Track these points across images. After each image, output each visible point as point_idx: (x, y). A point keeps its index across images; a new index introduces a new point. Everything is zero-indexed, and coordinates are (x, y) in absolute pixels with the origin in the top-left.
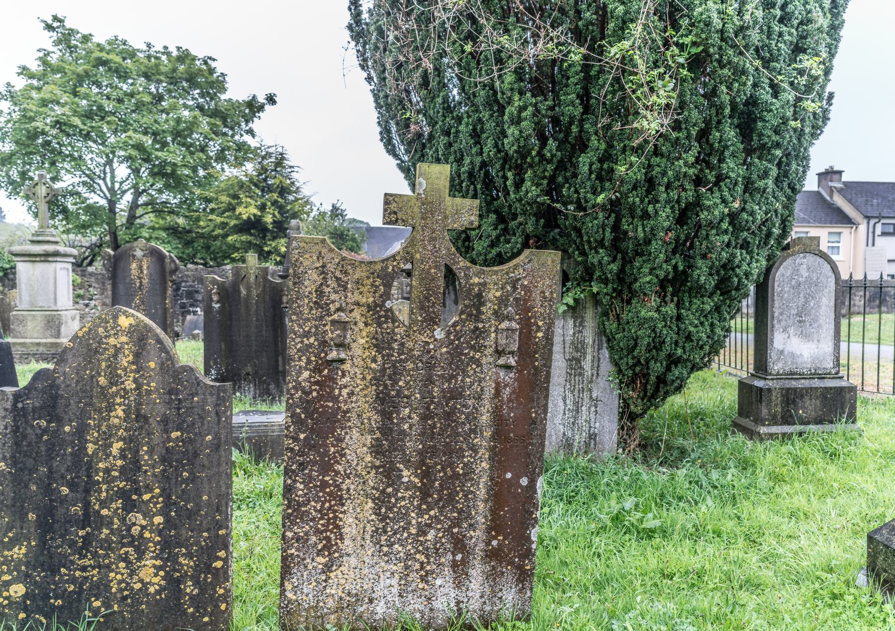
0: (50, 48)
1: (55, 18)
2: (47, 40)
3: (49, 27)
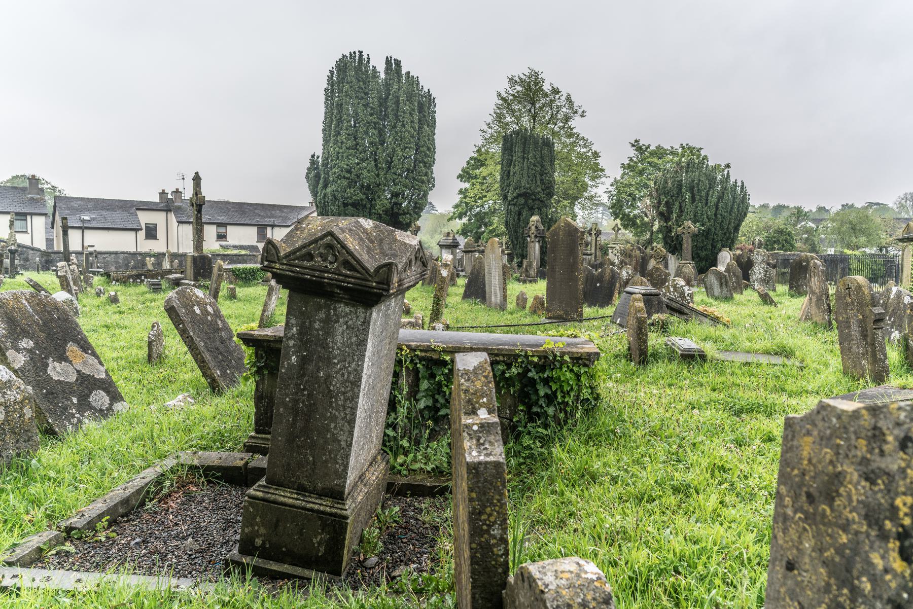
0: (632, 155)
1: (636, 141)
2: (632, 152)
3: (633, 146)
